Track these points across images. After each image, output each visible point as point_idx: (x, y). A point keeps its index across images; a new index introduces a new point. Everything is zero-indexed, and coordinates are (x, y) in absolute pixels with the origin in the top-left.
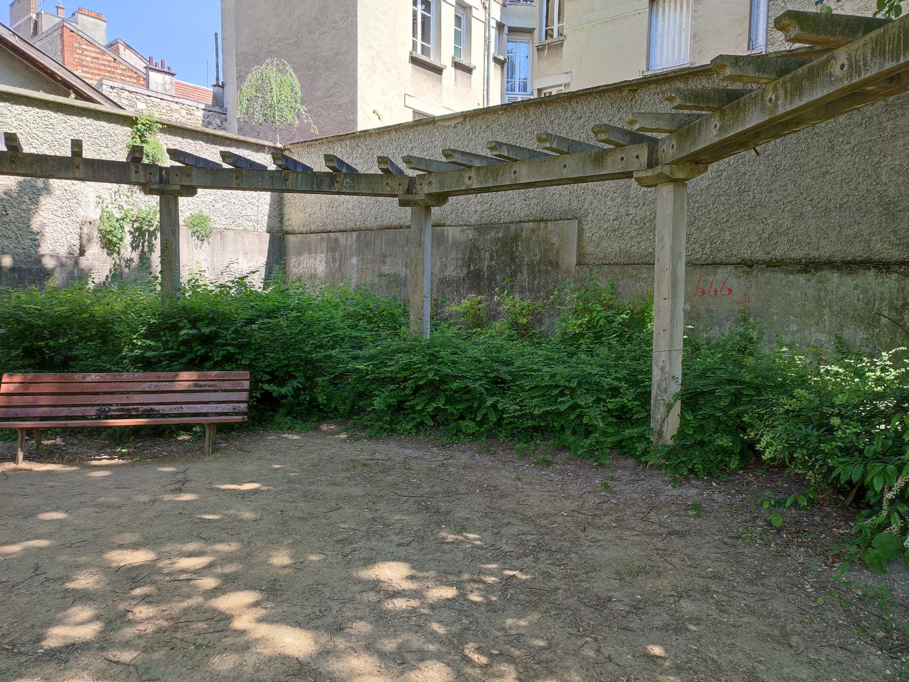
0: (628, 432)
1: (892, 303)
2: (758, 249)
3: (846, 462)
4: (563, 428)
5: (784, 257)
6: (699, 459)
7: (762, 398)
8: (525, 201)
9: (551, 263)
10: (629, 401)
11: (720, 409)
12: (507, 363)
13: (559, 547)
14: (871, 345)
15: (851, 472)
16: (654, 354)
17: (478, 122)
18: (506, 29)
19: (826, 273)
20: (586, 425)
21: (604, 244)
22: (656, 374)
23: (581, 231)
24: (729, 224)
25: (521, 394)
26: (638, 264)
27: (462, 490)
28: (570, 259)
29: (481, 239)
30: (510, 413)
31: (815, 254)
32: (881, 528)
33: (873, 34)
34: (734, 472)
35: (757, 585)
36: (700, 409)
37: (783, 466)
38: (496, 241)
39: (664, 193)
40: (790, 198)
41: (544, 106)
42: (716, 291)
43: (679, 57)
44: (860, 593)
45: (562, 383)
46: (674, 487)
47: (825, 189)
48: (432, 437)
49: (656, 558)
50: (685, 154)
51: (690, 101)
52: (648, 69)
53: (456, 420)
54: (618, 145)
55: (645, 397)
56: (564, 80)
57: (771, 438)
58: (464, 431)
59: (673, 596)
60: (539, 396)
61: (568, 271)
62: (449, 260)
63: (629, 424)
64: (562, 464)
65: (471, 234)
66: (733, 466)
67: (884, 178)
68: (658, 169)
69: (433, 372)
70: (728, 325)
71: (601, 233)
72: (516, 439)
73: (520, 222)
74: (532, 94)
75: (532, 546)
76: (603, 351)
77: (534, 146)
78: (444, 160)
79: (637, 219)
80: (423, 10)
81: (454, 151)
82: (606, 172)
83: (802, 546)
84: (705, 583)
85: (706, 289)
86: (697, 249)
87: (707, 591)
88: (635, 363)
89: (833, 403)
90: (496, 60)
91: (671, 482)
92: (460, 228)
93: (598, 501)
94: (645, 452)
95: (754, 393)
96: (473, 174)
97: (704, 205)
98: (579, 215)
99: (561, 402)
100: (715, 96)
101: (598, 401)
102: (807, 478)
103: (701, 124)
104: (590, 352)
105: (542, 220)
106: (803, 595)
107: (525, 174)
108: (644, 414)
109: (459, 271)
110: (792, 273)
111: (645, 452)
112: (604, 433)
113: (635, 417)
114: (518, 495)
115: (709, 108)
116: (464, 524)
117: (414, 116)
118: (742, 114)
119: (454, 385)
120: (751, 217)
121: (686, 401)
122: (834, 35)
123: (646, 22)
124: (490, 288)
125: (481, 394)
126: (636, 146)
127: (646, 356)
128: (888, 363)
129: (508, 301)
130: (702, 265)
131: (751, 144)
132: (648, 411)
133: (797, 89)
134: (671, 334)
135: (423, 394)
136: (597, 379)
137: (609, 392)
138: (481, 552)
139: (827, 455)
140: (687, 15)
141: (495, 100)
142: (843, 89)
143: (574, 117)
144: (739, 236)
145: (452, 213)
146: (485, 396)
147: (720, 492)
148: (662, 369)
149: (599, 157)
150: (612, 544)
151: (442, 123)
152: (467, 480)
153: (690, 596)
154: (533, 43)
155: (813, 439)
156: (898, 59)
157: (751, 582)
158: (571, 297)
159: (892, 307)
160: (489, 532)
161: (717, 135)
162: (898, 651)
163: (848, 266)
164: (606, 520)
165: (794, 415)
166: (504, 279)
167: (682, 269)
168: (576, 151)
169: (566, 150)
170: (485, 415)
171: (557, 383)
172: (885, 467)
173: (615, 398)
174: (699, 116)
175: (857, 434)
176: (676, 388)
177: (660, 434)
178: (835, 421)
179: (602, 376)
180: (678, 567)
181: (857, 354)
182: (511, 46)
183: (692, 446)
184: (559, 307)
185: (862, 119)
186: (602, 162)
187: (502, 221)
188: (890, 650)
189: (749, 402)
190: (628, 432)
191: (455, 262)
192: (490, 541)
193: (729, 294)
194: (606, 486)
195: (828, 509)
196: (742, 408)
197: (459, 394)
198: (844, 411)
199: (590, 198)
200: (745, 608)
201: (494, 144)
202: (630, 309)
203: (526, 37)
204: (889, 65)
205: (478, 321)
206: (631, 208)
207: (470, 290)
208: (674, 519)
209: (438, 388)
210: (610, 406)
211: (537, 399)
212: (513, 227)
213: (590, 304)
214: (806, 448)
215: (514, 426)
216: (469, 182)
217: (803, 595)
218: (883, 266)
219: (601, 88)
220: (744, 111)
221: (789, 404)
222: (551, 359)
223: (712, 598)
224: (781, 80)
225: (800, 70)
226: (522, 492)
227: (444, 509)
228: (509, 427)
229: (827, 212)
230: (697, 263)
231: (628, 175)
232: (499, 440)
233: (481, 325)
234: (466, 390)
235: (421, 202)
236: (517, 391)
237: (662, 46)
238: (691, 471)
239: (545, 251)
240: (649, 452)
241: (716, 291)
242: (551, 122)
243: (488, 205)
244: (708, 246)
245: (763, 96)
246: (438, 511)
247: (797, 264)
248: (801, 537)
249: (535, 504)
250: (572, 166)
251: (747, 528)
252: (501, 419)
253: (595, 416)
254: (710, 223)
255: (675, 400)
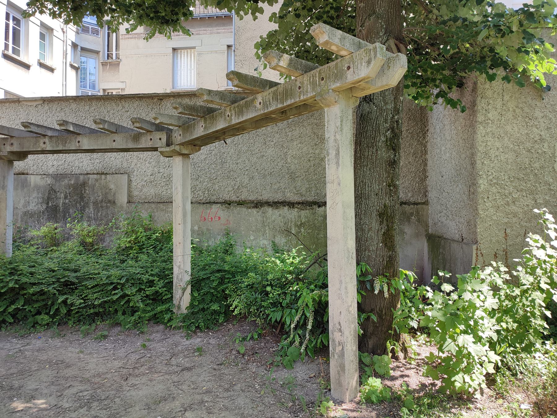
0: (159, 309)
1: (296, 223)
2: (233, 194)
3: (274, 311)
4: (116, 311)
5: (246, 199)
6: (202, 319)
7: (235, 279)
8: (91, 160)
9: (110, 201)
10: (160, 288)
11: (213, 288)
12: (76, 271)
13: (107, 396)
14: (288, 246)
15: (276, 316)
16: (174, 258)
17: (54, 106)
18: (79, 48)
19: (266, 208)
20: (132, 307)
21: (145, 190)
22: (176, 270)
23: (130, 181)
24: (217, 180)
25: (85, 292)
26: (167, 202)
27: (34, 367)
28: (123, 199)
29: (57, 184)
30: (77, 306)
31: (260, 198)
32: (292, 343)
33: (273, 89)
34: (222, 324)
35: (230, 391)
36: (202, 289)
37: (245, 317)
38: (69, 186)
39: (177, 162)
40: (247, 168)
41: (103, 101)
42: (212, 218)
43: (191, 84)
44: (281, 383)
45: (115, 281)
46: (187, 339)
47: (263, 164)
48: (12, 331)
49: (173, 388)
50: (187, 140)
51: (187, 111)
52: (173, 88)
53: (33, 316)
54: (148, 131)
55: (169, 285)
56: (121, 86)
57: (238, 302)
58: (40, 322)
59: (181, 411)
60: (99, 291)
61: (122, 207)
62: (31, 198)
63: (161, 303)
64: (115, 336)
65: (49, 181)
66: (220, 321)
67: (289, 160)
68: (172, 147)
69: (13, 282)
70: (219, 237)
71: (143, 183)
72: (82, 323)
73: (87, 174)
74: (99, 91)
75: (88, 399)
76: (143, 257)
77: (94, 126)
78: (23, 128)
79: (165, 175)
80: (14, 24)
81: (30, 124)
82: (141, 147)
83: (255, 362)
84: (201, 398)
85: (206, 217)
86: (200, 194)
87: (202, 402)
88: (164, 264)
89: (267, 279)
90: (72, 66)
91: (185, 337)
92: (40, 176)
93: (138, 357)
94: (170, 320)
95: (231, 277)
96: (47, 140)
97: (203, 169)
98: (128, 172)
99: (114, 294)
100: (201, 110)
101: (140, 290)
102: (257, 322)
103: (194, 125)
104: (136, 260)
105: (103, 174)
106: (254, 391)
107: (86, 143)
108: (169, 296)
109: (40, 206)
110: (250, 208)
111: (170, 320)
112: (144, 311)
113: (164, 298)
114: (79, 364)
115: (198, 116)
116: (33, 394)
117: (5, 95)
118: (215, 122)
119: (31, 291)
120: (228, 177)
121: (194, 285)
122: (255, 87)
123: (171, 61)
124: (65, 218)
125: (55, 294)
126: (159, 133)
127: (170, 260)
128: (295, 254)
129: (78, 227)
130: (204, 203)
131: (222, 138)
132: (172, 293)
133: (240, 112)
134: (184, 246)
135: (5, 299)
136: (139, 276)
137: (147, 284)
138: (45, 413)
139: (266, 308)
140: (194, 62)
141: (72, 92)
142: (261, 115)
143: (123, 110)
144: (223, 188)
145: (34, 165)
146: (57, 295)
147: (213, 338)
148: (179, 267)
149: (136, 137)
150: (145, 385)
151: (25, 103)
152: (39, 359)
153: (191, 409)
154: (99, 60)
155: (258, 300)
156: (283, 104)
157: (227, 390)
158: (123, 223)
159: (296, 225)
160: (54, 396)
161: (203, 131)
162: (298, 412)
163: (276, 204)
164: (142, 369)
165: (251, 286)
166: (75, 212)
167: (189, 206)
168: (122, 132)
169: (115, 131)
170: (58, 310)
171: (112, 281)
172: (291, 311)
173: (151, 287)
174: (194, 119)
175: (279, 295)
176: (188, 278)
177: (179, 307)
178: (269, 289)
179: (143, 274)
180: (186, 391)
181: (282, 250)
182: (83, 59)
183: (197, 312)
184: (115, 230)
185: (278, 130)
186: (139, 140)
187: (73, 173)
188: (294, 412)
189: (229, 282)
190: (159, 309)
191: (36, 200)
192: (54, 402)
193: (219, 220)
194: (144, 346)
195: (268, 338)
196: (225, 286)
197: (36, 296)
198: (273, 282)
199: (135, 161)
200: (223, 407)
201: (62, 122)
202: (161, 230)
203: (95, 55)
204: (280, 106)
205: (55, 242)
206: (161, 169)
207: (49, 219)
208: (186, 360)
209: (18, 293)
210: (148, 293)
211: (97, 294)
212: (82, 177)
213: (136, 228)
214: (256, 306)
215: (80, 314)
216: (44, 146)
217: (254, 391)
218: (291, 205)
219: (141, 95)
220: (216, 120)
221: (246, 282)
222: (108, 265)
223: (205, 406)
224: (233, 106)
225: (241, 102)
226: (83, 361)
227: (16, 386)
228: (77, 315)
229: (264, 176)
230: (201, 202)
231: (155, 149)
232: (69, 326)
233: (57, 245)
234: (42, 293)
235: (3, 157)
236: (82, 290)
237: (181, 76)
238: (197, 327)
239: (106, 194)
240: (173, 320)
241: (212, 218)
242: (108, 112)
243: (63, 162)
244: (207, 192)
245: (224, 113)
246: (11, 388)
247: (252, 203)
248: (254, 357)
249: (92, 368)
250: (120, 141)
251: (227, 357)
252: (69, 311)
253: (137, 301)
254: (207, 180)
255: (187, 285)
